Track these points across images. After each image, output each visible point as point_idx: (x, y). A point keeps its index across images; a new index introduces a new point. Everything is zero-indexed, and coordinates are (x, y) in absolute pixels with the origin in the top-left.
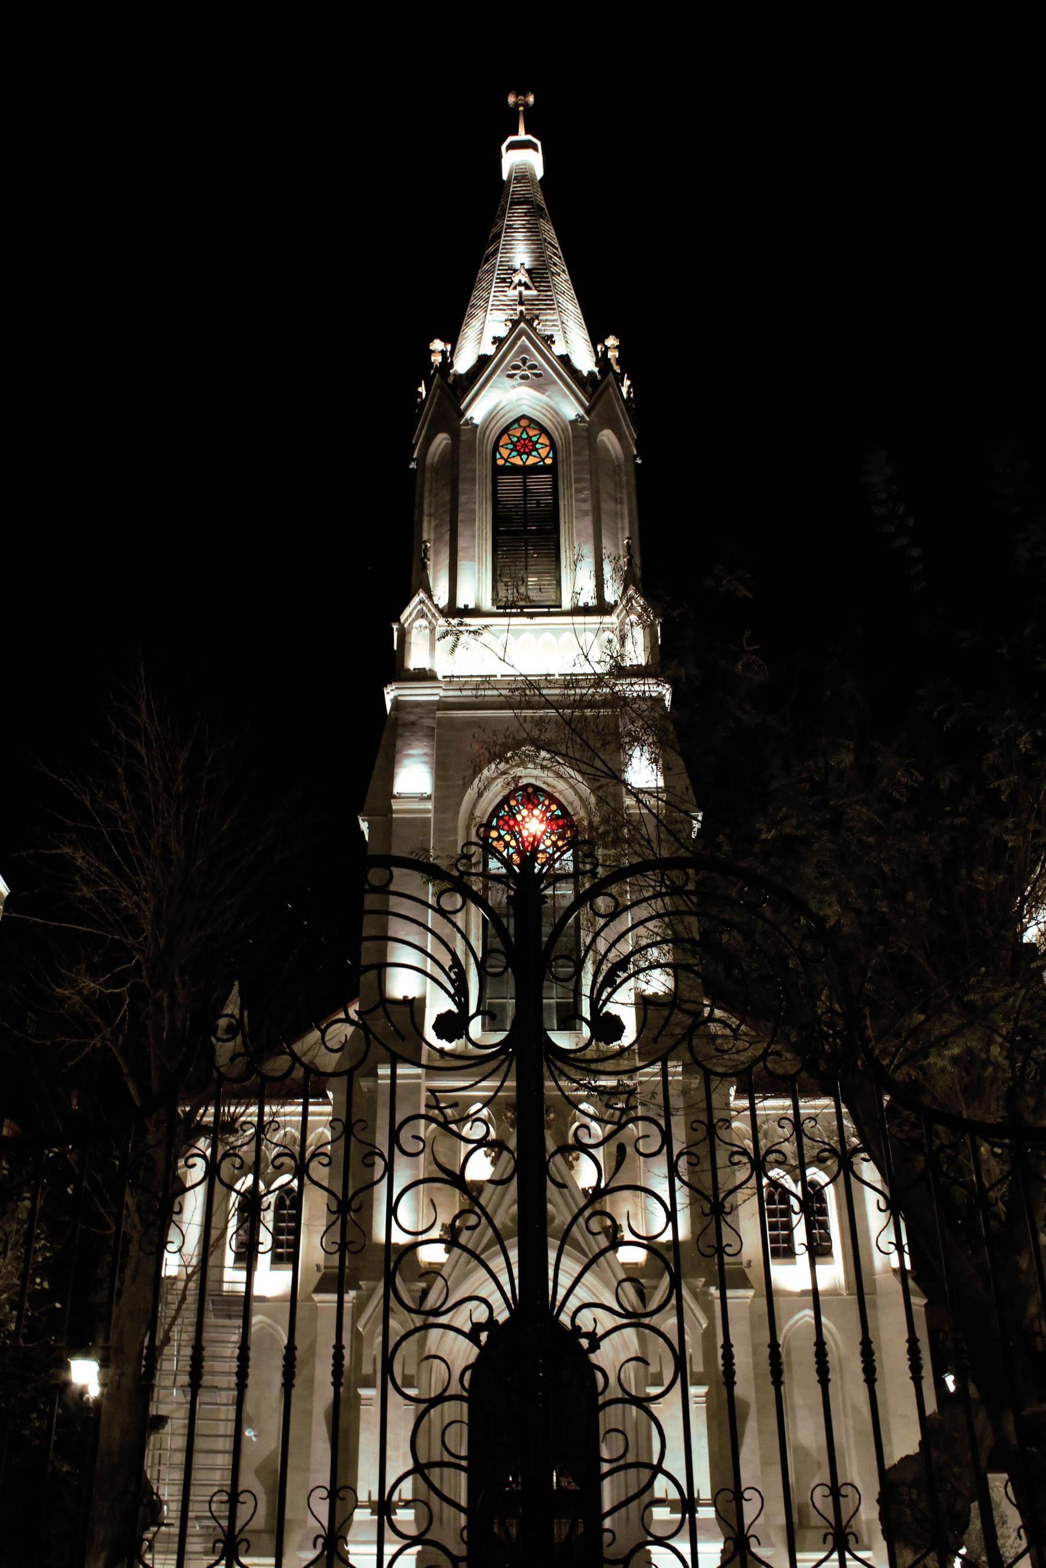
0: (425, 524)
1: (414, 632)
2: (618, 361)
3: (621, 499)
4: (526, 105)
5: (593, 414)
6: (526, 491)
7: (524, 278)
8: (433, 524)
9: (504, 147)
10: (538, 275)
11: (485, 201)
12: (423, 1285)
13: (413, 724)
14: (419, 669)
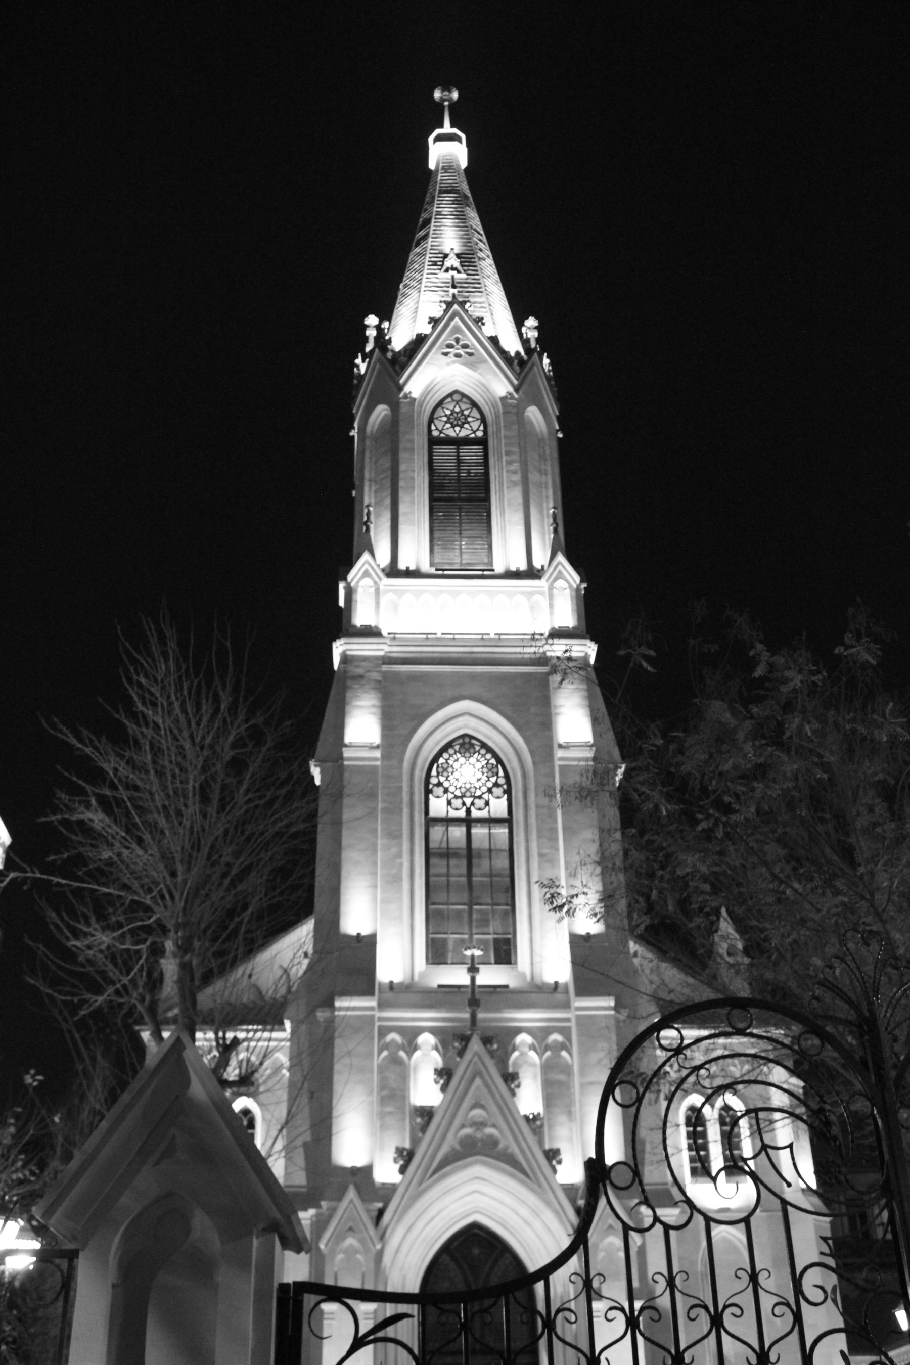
1: (360, 590)
2: (538, 340)
3: (546, 470)
4: (450, 100)
5: (521, 392)
6: (459, 461)
7: (456, 263)
8: (373, 488)
9: (431, 139)
10: (467, 259)
11: (413, 190)
12: (380, 1205)
13: (361, 677)
14: (366, 626)
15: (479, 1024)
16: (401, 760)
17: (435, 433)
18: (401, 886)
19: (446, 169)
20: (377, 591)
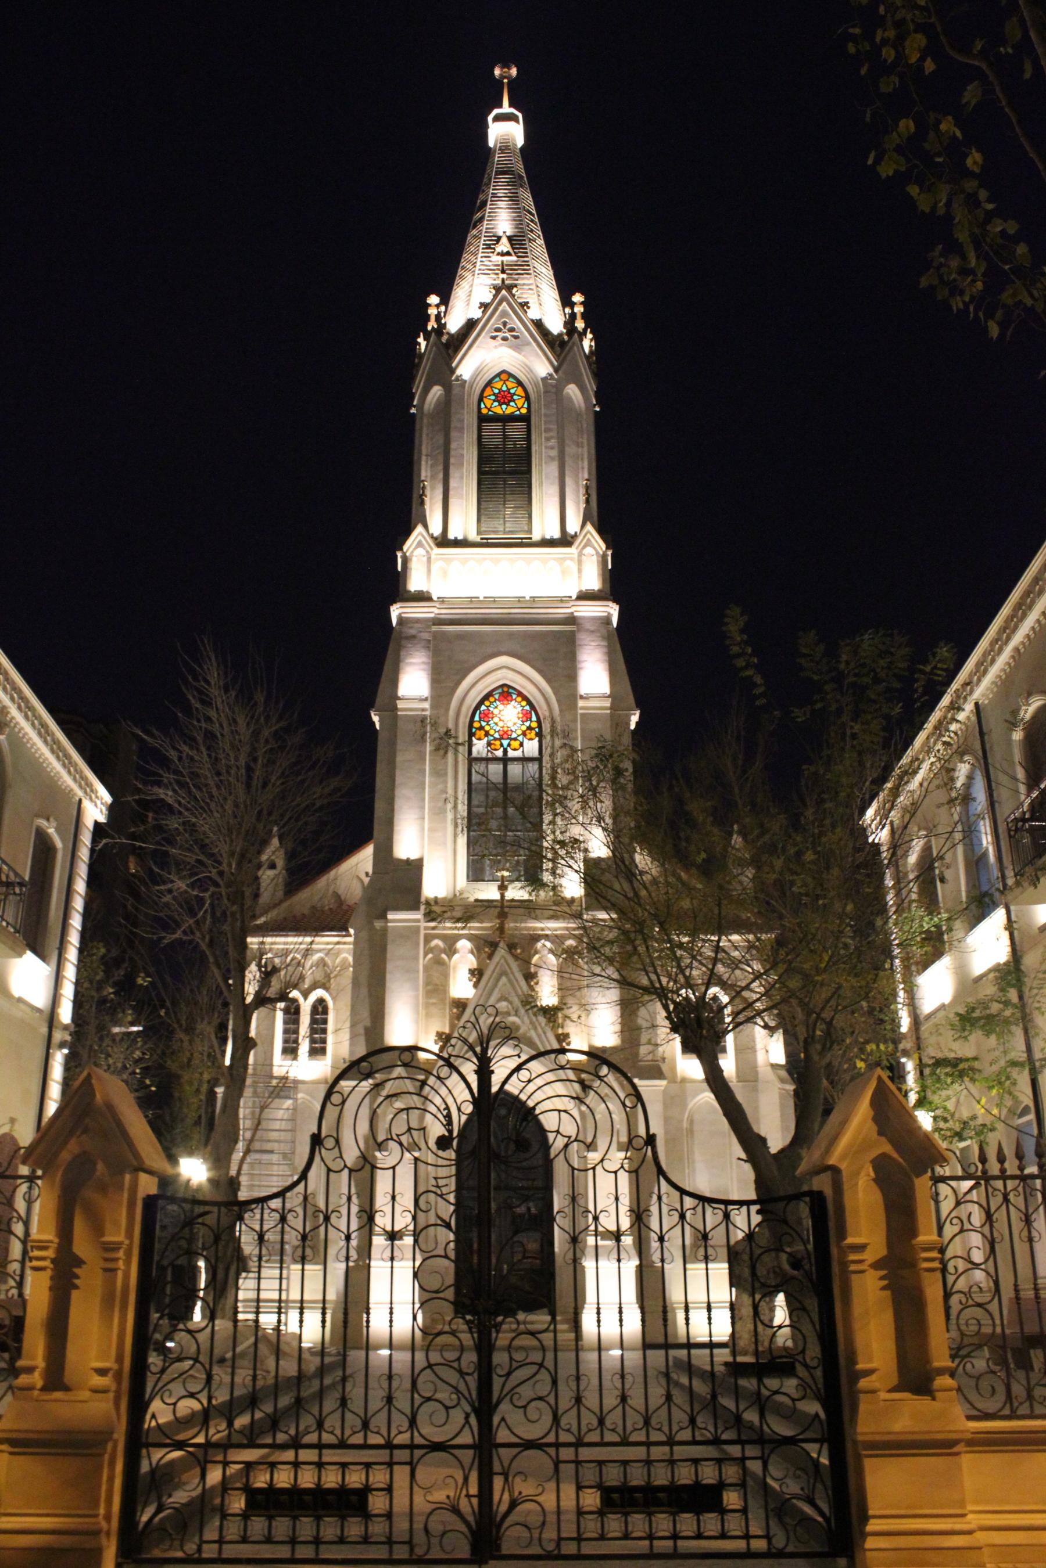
0: (423, 463)
1: (414, 559)
6: (505, 437)
9: (490, 118)
10: (517, 242)
13: (414, 637)
15: (507, 932)
16: (448, 709)
17: (484, 411)
18: (445, 817)
19: (502, 150)
20: (429, 560)
